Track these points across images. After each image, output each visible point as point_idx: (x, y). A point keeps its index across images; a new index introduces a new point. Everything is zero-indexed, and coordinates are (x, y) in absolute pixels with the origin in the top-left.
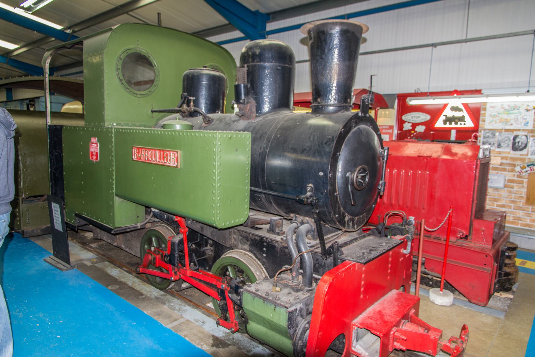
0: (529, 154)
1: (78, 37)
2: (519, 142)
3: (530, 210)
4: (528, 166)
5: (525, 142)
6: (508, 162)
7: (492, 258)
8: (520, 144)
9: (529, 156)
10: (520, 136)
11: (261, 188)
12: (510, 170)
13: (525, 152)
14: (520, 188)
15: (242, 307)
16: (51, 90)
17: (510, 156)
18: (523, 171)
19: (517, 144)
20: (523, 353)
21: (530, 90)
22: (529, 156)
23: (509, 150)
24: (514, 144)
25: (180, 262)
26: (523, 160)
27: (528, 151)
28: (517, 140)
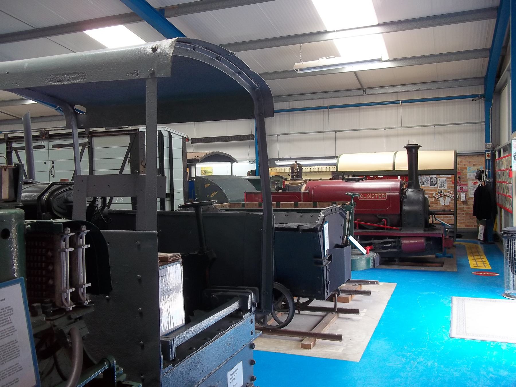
0: (438, 187)
1: (187, 37)
2: (433, 181)
3: (442, 217)
4: (439, 193)
5: (436, 181)
6: (429, 192)
7: (54, 208)
8: (433, 182)
9: (439, 188)
10: (433, 178)
11: (358, 241)
12: (430, 197)
13: (436, 186)
14: (436, 206)
15: (365, 86)
16: (231, 137)
17: (429, 189)
18: (437, 196)
19: (432, 182)
20: (1, 34)
21: (255, 343)
22: (439, 188)
23: (428, 185)
24: (431, 182)
25: (436, 184)
26: (436, 191)
27: (438, 186)
28: (432, 180)
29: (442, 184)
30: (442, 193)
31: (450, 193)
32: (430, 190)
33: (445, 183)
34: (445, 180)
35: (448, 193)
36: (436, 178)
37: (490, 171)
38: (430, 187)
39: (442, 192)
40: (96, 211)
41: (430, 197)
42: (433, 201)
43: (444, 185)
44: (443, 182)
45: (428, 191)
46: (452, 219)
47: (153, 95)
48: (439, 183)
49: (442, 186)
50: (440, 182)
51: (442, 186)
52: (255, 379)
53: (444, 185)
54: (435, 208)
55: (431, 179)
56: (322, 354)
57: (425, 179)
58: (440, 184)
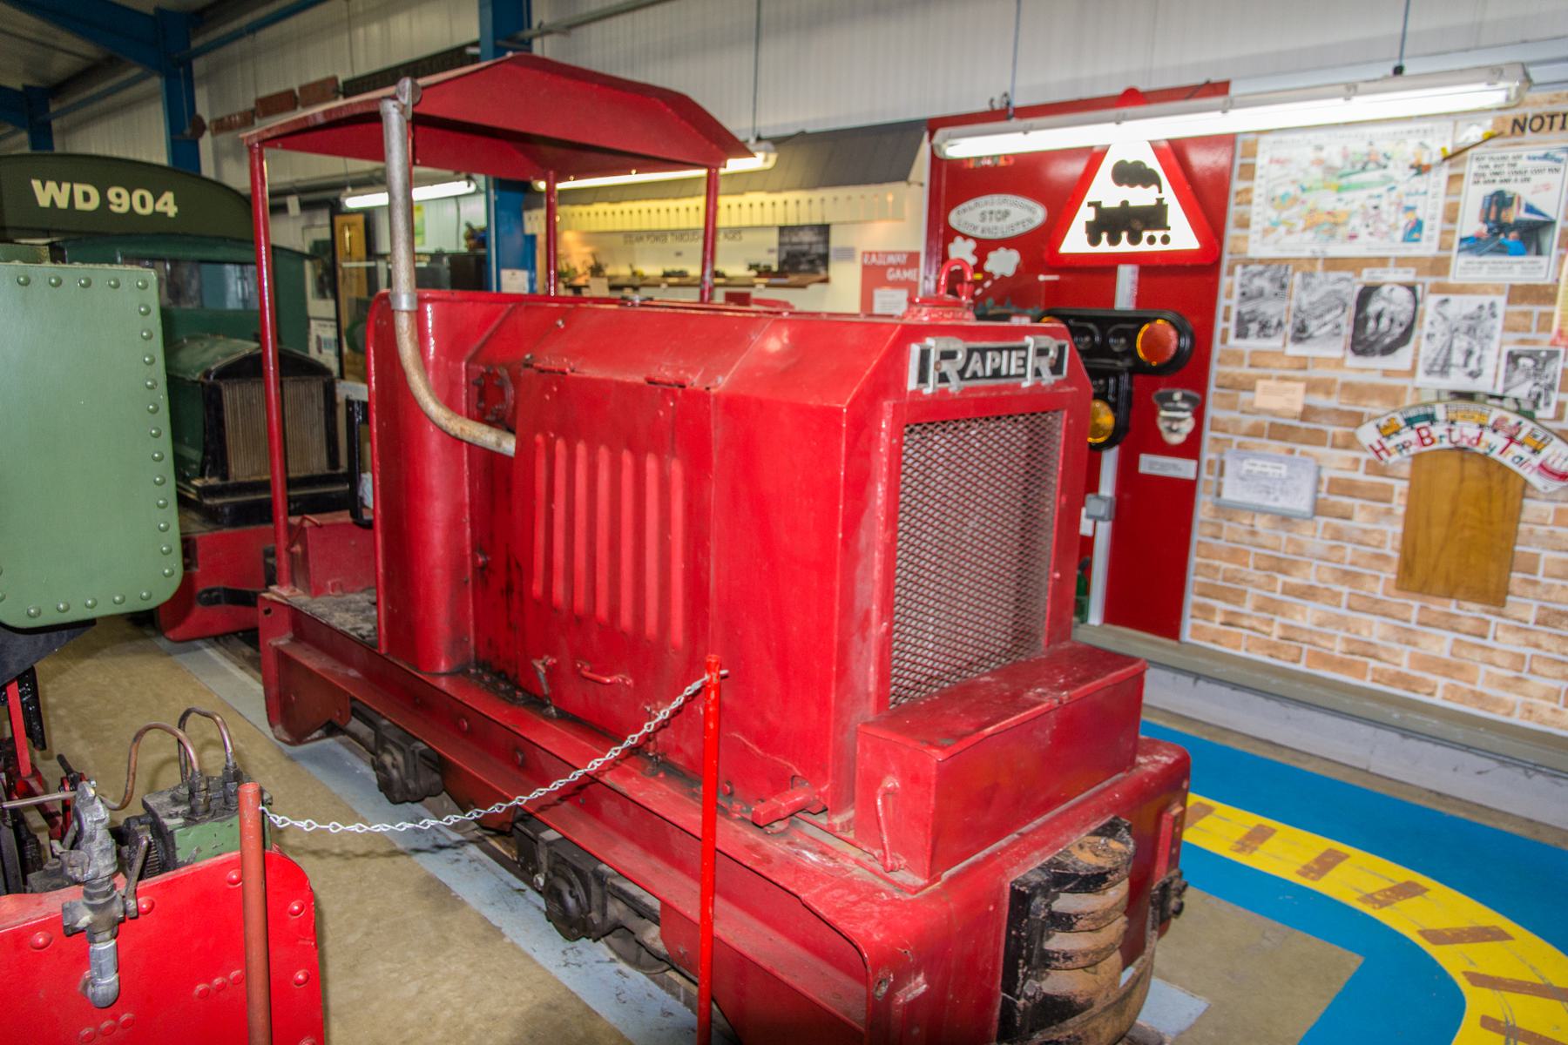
2: (1379, 316)
3: (1414, 615)
4: (1410, 422)
5: (1404, 317)
8: (1384, 322)
9: (1421, 379)
10: (1385, 290)
12: (1339, 441)
13: (1402, 359)
17: (1341, 376)
18: (1389, 444)
23: (1337, 349)
24: (1360, 323)
25: (1405, 338)
28: (1373, 308)
29: (1461, 343)
30: (1438, 430)
31: (1512, 439)
32: (1347, 387)
33: (1489, 337)
34: (1486, 313)
35: (1488, 436)
36: (1411, 288)
37: (1363, 677)
38: (1353, 361)
39: (1431, 418)
40: (145, 892)
41: (1339, 441)
42: (1360, 476)
43: (1469, 353)
44: (1473, 325)
45: (1328, 393)
46: (1492, 649)
47: (172, 703)
48: (1429, 336)
49: (1457, 358)
50: (1440, 328)
51: (1457, 358)
52: (1412, 167)
53: (1469, 353)
54: (1365, 531)
55: (1367, 294)
56: (1113, 885)
57: (1314, 298)
58: (1439, 341)
